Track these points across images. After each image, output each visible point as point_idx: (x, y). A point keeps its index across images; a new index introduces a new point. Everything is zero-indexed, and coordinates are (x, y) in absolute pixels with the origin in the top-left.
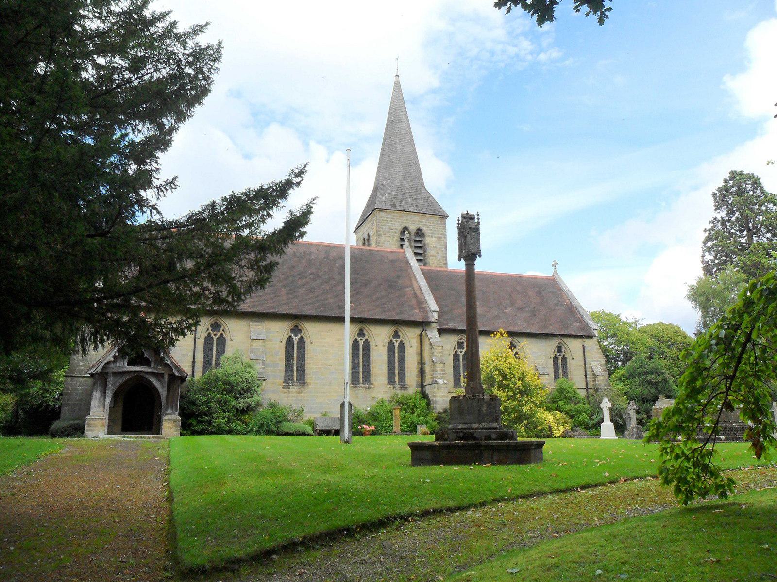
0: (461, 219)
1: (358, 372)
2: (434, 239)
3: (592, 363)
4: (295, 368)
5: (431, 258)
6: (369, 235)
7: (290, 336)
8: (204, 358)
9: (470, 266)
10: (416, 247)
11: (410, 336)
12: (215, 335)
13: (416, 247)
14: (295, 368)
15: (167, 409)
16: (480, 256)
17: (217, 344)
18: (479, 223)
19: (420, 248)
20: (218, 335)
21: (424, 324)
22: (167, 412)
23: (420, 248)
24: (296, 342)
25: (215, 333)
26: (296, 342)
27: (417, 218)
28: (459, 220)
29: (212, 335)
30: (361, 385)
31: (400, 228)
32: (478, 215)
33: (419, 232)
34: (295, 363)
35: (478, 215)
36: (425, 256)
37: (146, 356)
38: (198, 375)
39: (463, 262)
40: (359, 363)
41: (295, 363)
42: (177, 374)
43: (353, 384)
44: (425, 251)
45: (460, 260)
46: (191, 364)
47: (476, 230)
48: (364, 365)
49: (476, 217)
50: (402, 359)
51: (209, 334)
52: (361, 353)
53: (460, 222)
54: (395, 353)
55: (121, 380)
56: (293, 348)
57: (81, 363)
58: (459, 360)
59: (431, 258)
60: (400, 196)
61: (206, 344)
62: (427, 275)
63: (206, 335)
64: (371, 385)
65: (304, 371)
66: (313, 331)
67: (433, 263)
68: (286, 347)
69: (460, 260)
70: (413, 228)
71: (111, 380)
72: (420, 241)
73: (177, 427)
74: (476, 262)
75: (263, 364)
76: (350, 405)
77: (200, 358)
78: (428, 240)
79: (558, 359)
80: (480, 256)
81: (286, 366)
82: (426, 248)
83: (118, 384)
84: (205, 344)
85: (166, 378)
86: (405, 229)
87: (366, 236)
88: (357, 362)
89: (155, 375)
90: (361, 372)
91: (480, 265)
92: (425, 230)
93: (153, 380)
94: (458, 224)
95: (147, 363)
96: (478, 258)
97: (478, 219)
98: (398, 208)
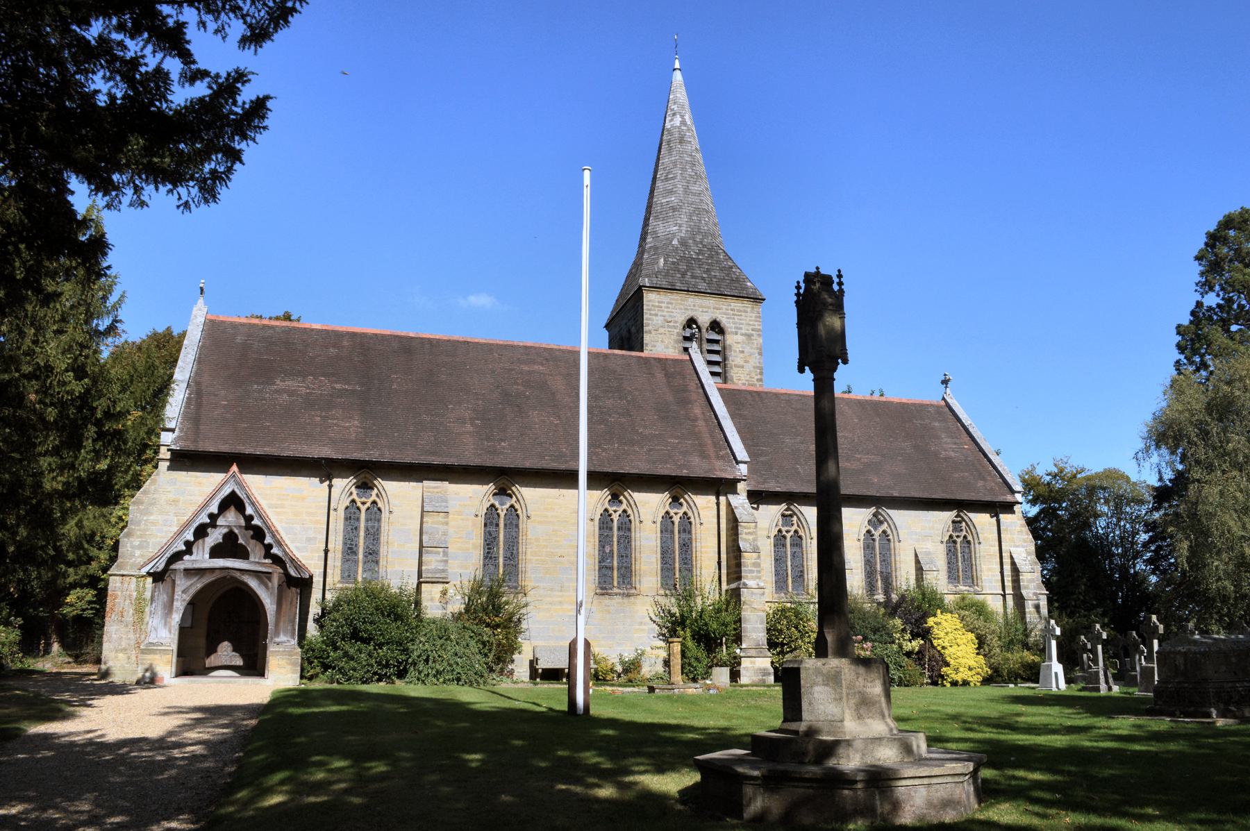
0: (803, 285)
1: (611, 568)
2: (739, 338)
3: (1013, 550)
4: (501, 560)
5: (735, 370)
6: (629, 331)
7: (492, 506)
8: (345, 544)
9: (824, 385)
10: (710, 352)
11: (704, 505)
12: (364, 503)
13: (710, 352)
14: (501, 560)
15: (277, 634)
16: (845, 362)
17: (367, 520)
18: (841, 291)
19: (717, 352)
20: (368, 505)
21: (721, 486)
22: (277, 640)
23: (717, 352)
24: (502, 515)
25: (364, 499)
26: (502, 515)
27: (710, 302)
28: (798, 287)
29: (359, 504)
30: (616, 590)
31: (682, 319)
32: (840, 276)
33: (716, 326)
34: (501, 552)
35: (840, 276)
36: (725, 366)
37: (241, 541)
38: (334, 576)
39: (808, 375)
40: (612, 551)
41: (501, 552)
42: (292, 572)
43: (602, 588)
44: (725, 359)
45: (801, 370)
46: (323, 554)
47: (121, 693)
48: (621, 556)
49: (836, 280)
50: (686, 546)
51: (353, 501)
52: (614, 544)
53: (802, 291)
54: (677, 538)
55: (198, 584)
56: (497, 525)
57: (138, 553)
58: (784, 546)
59: (735, 370)
60: (683, 267)
61: (347, 519)
62: (731, 397)
63: (348, 503)
64: (633, 591)
65: (516, 566)
66: (534, 499)
67: (742, 376)
68: (485, 525)
69: (801, 370)
70: (704, 320)
71: (181, 583)
72: (717, 342)
73: (294, 664)
74: (836, 375)
75: (445, 554)
76: (587, 644)
77: (337, 544)
78: (730, 339)
79: (955, 542)
80: (845, 362)
81: (485, 558)
82: (728, 353)
83: (193, 591)
84: (346, 519)
85: (276, 580)
86: (691, 322)
87: (625, 333)
88: (607, 550)
89: (256, 574)
90: (614, 571)
91: (843, 378)
92: (724, 322)
93: (253, 583)
94: (798, 295)
95: (243, 554)
96: (841, 366)
97: (840, 284)
98: (678, 285)
